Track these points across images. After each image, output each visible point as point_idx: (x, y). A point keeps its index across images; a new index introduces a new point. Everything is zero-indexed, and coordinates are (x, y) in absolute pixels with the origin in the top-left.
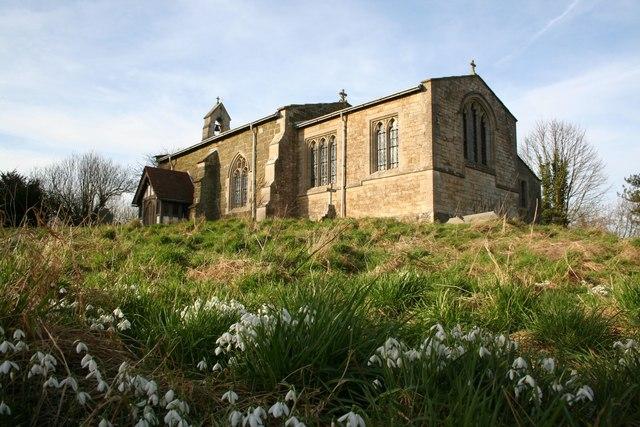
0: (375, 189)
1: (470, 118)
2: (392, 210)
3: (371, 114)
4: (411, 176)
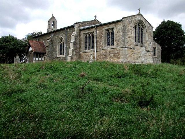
0: (106, 52)
1: (137, 29)
2: (111, 60)
3: (106, 27)
4: (117, 49)
